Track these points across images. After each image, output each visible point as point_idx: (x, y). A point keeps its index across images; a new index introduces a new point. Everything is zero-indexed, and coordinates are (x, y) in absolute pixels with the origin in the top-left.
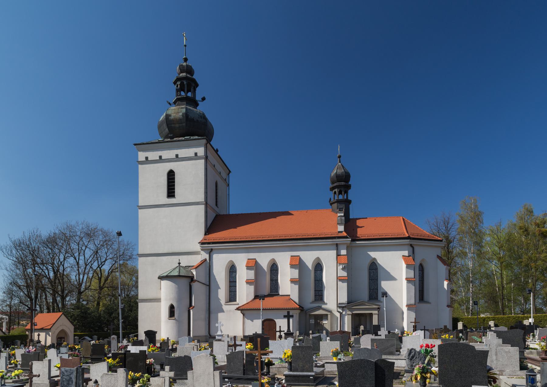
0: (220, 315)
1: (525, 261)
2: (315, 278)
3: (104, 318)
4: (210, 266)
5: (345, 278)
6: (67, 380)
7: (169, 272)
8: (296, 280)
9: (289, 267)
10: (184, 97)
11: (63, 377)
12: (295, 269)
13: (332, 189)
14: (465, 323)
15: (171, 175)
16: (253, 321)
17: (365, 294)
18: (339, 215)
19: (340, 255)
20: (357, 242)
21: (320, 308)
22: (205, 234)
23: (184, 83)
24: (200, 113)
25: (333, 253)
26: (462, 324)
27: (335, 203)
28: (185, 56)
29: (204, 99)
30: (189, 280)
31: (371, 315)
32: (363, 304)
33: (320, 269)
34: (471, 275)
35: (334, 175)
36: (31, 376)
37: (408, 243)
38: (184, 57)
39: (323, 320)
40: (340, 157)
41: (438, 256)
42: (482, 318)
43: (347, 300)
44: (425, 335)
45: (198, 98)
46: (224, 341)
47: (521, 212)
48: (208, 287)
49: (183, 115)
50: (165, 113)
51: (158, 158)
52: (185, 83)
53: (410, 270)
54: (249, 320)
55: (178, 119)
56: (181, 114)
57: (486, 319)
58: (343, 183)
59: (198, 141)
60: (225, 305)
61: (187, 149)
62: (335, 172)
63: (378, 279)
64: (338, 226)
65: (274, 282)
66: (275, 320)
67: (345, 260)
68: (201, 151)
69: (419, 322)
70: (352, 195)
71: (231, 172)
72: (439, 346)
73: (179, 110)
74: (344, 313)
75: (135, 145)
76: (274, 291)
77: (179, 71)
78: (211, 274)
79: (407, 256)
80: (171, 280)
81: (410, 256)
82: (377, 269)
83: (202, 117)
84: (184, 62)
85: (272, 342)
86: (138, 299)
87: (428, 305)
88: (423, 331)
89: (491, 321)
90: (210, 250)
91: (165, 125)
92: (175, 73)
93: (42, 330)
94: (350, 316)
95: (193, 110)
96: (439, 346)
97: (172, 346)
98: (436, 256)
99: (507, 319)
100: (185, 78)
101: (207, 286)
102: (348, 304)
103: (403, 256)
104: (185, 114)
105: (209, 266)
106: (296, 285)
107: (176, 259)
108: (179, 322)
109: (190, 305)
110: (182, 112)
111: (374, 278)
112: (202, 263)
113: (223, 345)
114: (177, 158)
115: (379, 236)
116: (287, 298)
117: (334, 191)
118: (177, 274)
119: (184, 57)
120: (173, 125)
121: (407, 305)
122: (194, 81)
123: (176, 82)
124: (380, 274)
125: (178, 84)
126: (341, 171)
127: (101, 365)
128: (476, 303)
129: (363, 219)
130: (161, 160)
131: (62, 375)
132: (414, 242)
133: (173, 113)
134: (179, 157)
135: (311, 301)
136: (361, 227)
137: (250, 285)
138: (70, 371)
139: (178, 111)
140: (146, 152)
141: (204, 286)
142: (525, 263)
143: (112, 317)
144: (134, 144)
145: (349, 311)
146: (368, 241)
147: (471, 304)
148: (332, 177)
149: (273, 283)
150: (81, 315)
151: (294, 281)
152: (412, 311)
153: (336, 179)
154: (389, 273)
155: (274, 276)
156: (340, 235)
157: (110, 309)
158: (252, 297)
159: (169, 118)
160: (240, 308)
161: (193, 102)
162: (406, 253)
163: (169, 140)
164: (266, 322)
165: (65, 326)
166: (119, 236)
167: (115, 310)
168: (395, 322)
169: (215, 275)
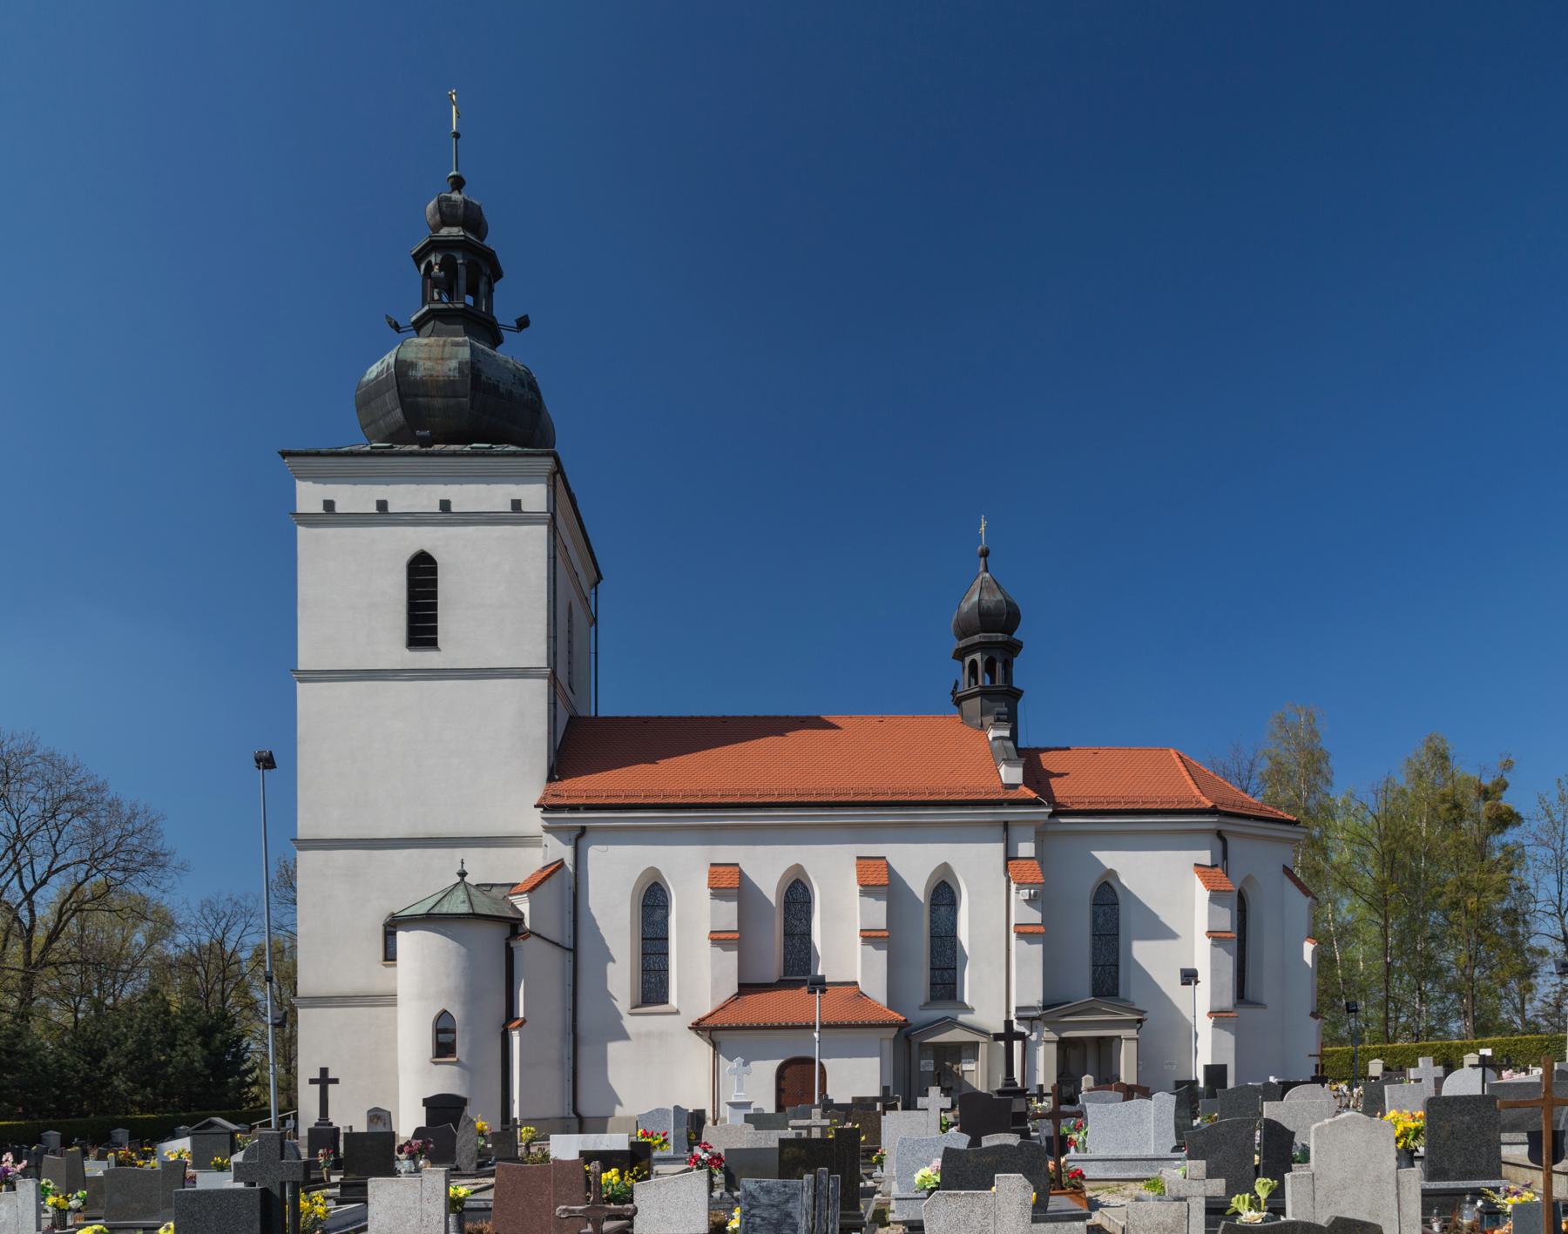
0: (614, 1049)
1: (1451, 892)
2: (931, 929)
3: (73, 1068)
5: (1036, 929)
6: (770, 1223)
8: (880, 934)
11: (752, 1212)
12: (877, 900)
13: (960, 655)
15: (422, 571)
17: (1081, 983)
19: (1017, 858)
21: (952, 1024)
22: (550, 779)
23: (455, 259)
24: (518, 369)
28: (457, 170)
29: (523, 323)
32: (1093, 1008)
33: (948, 901)
35: (971, 609)
36: (599, 1212)
37: (1212, 826)
38: (454, 173)
40: (985, 554)
42: (1348, 1052)
43: (1041, 998)
45: (504, 313)
46: (927, 1109)
47: (1417, 755)
48: (570, 956)
49: (460, 370)
50: (395, 351)
52: (460, 261)
53: (1220, 908)
56: (453, 364)
58: (1000, 637)
60: (630, 1014)
61: (485, 486)
62: (975, 598)
63: (1118, 935)
65: (796, 941)
68: (535, 496)
73: (447, 349)
74: (1034, 1037)
76: (796, 968)
77: (438, 217)
79: (1208, 867)
80: (443, 930)
81: (1216, 866)
83: (526, 384)
85: (1099, 1107)
87: (1260, 1011)
89: (1372, 1059)
90: (578, 832)
91: (390, 398)
94: (1054, 1046)
97: (527, 1147)
101: (567, 952)
102: (1045, 1007)
103: (1196, 865)
104: (470, 365)
105: (572, 883)
109: (507, 1018)
110: (456, 358)
111: (1106, 933)
112: (545, 879)
113: (923, 1120)
115: (1108, 803)
116: (850, 991)
117: (968, 660)
118: (464, 909)
119: (451, 174)
120: (420, 399)
121: (1211, 1014)
122: (490, 257)
123: (420, 255)
124: (1126, 916)
125: (433, 261)
126: (995, 596)
127: (680, 1182)
128: (1355, 1008)
129: (1057, 752)
131: (749, 1204)
132: (1228, 823)
133: (425, 359)
134: (453, 510)
135: (922, 1004)
136: (1060, 775)
137: (725, 950)
138: (783, 1189)
139: (443, 352)
140: (325, 484)
141: (557, 951)
142: (1451, 898)
143: (106, 1066)
145: (1051, 1030)
146: (1095, 818)
149: (793, 945)
152: (1226, 1030)
153: (978, 621)
154: (1156, 917)
155: (797, 922)
156: (1013, 795)
157: (92, 1037)
160: (705, 1024)
161: (484, 328)
162: (1205, 857)
163: (416, 447)
166: (265, 767)
167: (115, 1041)
168: (1171, 1064)
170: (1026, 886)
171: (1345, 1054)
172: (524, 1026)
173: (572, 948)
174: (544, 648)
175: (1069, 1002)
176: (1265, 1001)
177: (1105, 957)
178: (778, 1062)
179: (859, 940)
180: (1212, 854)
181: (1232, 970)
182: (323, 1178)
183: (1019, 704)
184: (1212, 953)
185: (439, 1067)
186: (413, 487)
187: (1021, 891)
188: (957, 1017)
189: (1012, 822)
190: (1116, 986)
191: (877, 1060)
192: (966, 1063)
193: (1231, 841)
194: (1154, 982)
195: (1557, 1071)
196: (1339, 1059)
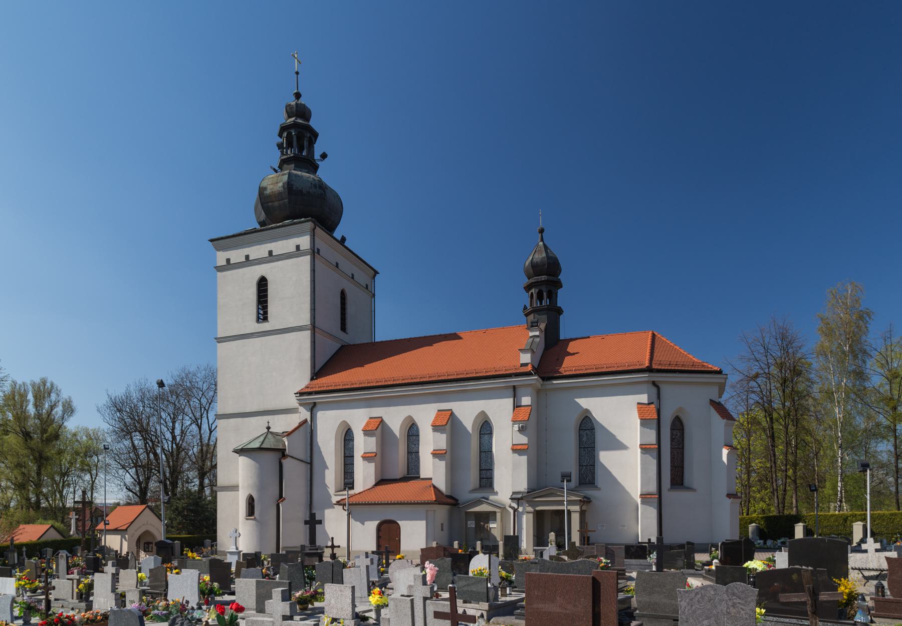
4: (312, 430)
7: (243, 445)
8: (441, 452)
9: (363, 435)
10: (291, 157)
13: (528, 288)
14: (809, 524)
15: (262, 284)
16: (363, 524)
18: (531, 334)
19: (521, 406)
20: (555, 382)
22: (312, 379)
23: (292, 133)
25: (507, 403)
26: (802, 527)
27: (531, 314)
29: (324, 156)
30: (279, 455)
34: (839, 433)
37: (646, 379)
38: (295, 91)
39: (490, 522)
43: (526, 487)
44: (491, 563)
48: (309, 466)
49: (283, 186)
51: (244, 260)
52: (293, 134)
53: (648, 430)
55: (278, 193)
56: (281, 184)
57: (849, 518)
58: (544, 278)
61: (285, 241)
64: (521, 354)
66: (399, 522)
67: (524, 414)
69: (595, 531)
70: (563, 298)
71: (378, 273)
73: (279, 178)
74: (521, 509)
75: (211, 241)
76: (413, 471)
78: (314, 444)
79: (646, 404)
82: (594, 429)
83: (318, 186)
84: (295, 99)
86: (216, 486)
88: (488, 555)
92: (282, 118)
93: (116, 531)
94: (531, 515)
95: (302, 176)
98: (709, 401)
99: (890, 519)
100: (295, 125)
104: (287, 184)
106: (441, 462)
107: (262, 421)
108: (261, 525)
114: (271, 257)
120: (270, 204)
124: (599, 437)
130: (248, 261)
134: (274, 254)
135: (471, 489)
136: (574, 354)
141: (303, 464)
147: (839, 489)
148: (527, 267)
149: (412, 458)
150: (188, 507)
151: (438, 454)
154: (614, 436)
158: (372, 482)
159: (265, 193)
162: (644, 398)
164: (385, 525)
169: (320, 447)
170: (518, 423)
171: (840, 517)
172: (284, 502)
173: (309, 461)
174: (309, 315)
175: (546, 487)
176: (695, 487)
178: (377, 522)
179: (639, 450)
180: (648, 396)
181: (656, 469)
185: (248, 521)
186: (258, 246)
187: (515, 426)
189: (518, 385)
190: (594, 478)
191: (424, 522)
192: (491, 523)
193: (662, 387)
196: (836, 521)
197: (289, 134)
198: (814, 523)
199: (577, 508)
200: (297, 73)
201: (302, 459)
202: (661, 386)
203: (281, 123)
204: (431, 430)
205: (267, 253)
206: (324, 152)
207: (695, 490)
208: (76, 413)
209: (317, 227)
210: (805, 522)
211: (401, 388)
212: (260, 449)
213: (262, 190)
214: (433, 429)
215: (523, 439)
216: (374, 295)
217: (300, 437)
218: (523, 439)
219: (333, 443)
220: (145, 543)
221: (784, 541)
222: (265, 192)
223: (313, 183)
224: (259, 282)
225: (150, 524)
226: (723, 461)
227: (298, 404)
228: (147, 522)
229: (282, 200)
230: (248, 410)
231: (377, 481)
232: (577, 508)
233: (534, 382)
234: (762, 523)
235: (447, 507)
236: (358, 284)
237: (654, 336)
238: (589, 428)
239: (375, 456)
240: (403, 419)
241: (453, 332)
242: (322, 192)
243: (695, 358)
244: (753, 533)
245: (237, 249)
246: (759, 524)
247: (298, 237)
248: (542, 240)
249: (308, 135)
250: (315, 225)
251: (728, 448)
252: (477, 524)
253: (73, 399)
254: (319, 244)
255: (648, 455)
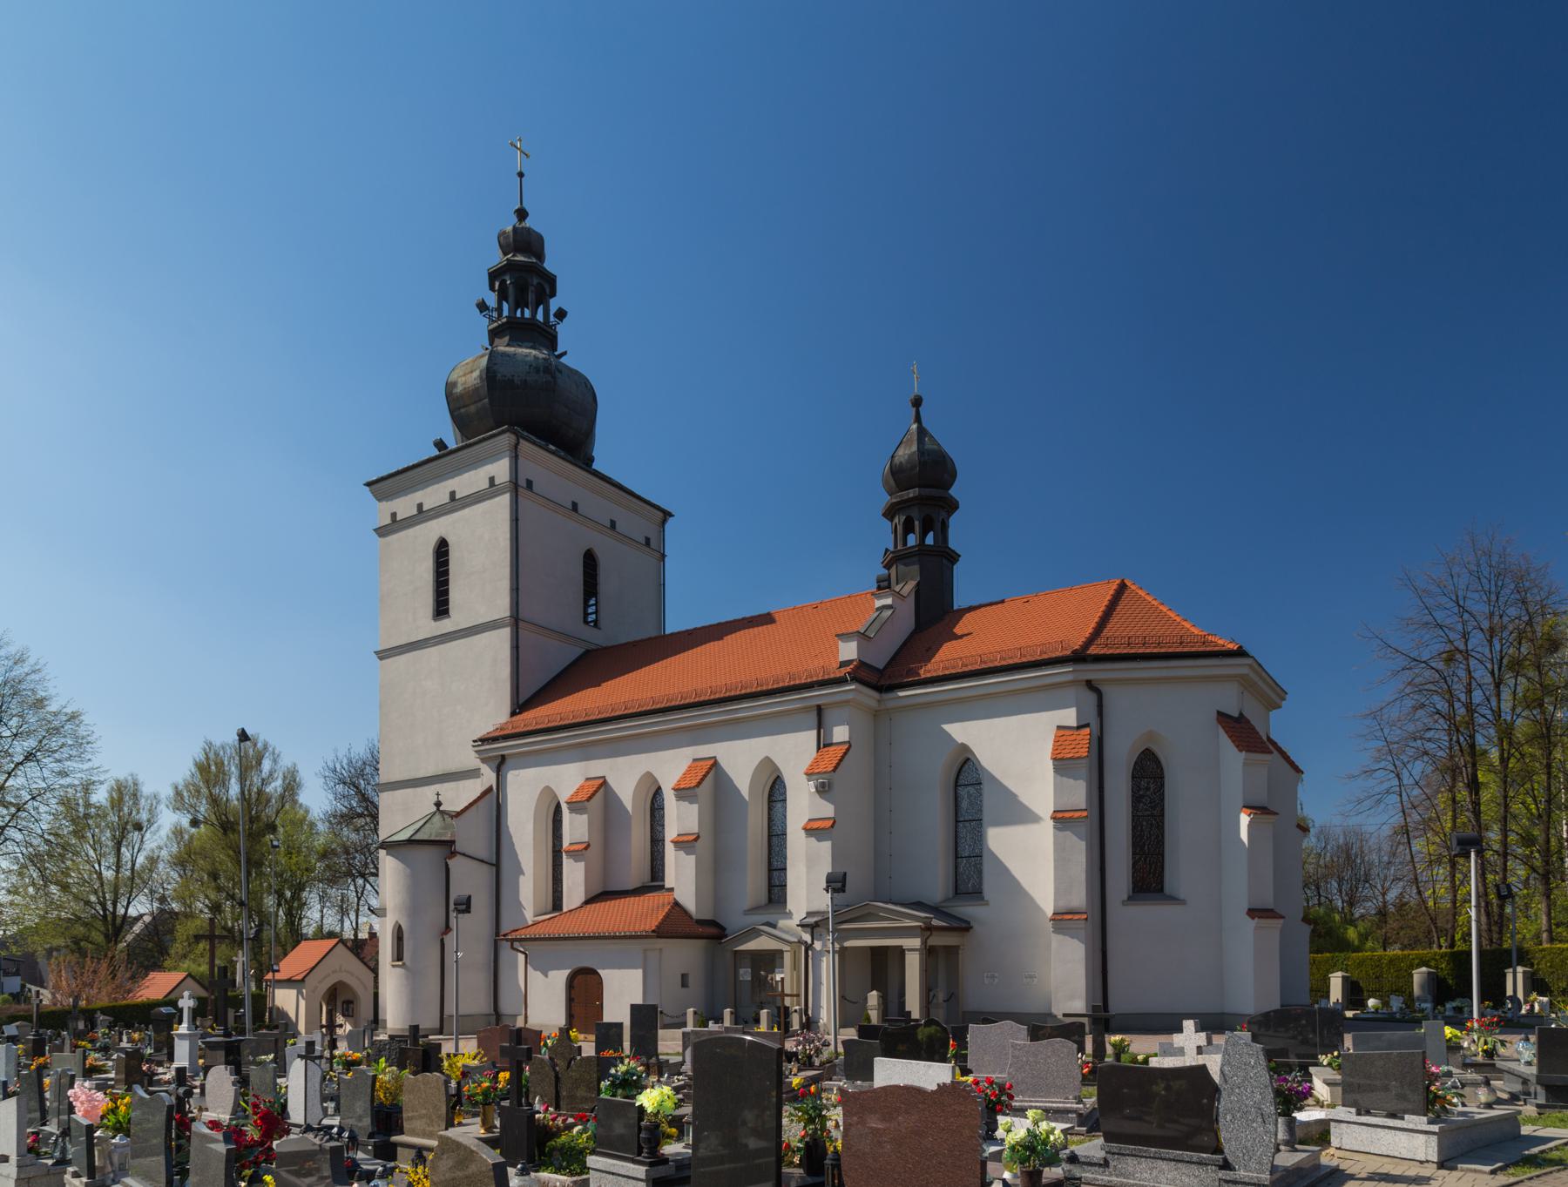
8: (1077, 814)
16: (546, 976)
18: (879, 603)
19: (831, 745)
20: (901, 694)
22: (513, 714)
27: (892, 565)
31: (901, 952)
37: (1070, 677)
39: (777, 970)
41: (1222, 717)
48: (494, 868)
49: (480, 377)
51: (415, 512)
52: (508, 282)
53: (1071, 781)
54: (539, 973)
56: (476, 374)
58: (912, 493)
59: (491, 441)
64: (840, 642)
70: (959, 533)
71: (671, 515)
72: (1204, 1067)
74: (818, 945)
75: (369, 484)
93: (289, 983)
96: (1204, 1067)
98: (1215, 715)
107: (428, 794)
114: (455, 503)
120: (463, 410)
135: (746, 908)
141: (485, 866)
144: (365, 485)
162: (1069, 716)
164: (580, 977)
165: (348, 972)
173: (494, 862)
177: (970, 845)
178: (566, 972)
181: (1084, 860)
182: (521, 1045)
183: (955, 567)
184: (1055, 837)
186: (436, 486)
188: (777, 922)
191: (638, 973)
194: (1014, 878)
195: (859, 1037)
197: (503, 283)
198: (1551, 966)
199: (916, 942)
200: (521, 175)
201: (480, 858)
202: (1105, 689)
203: (487, 268)
204: (673, 797)
205: (448, 496)
206: (560, 308)
207: (1182, 902)
208: (303, 789)
209: (521, 440)
210: (1532, 965)
211: (630, 721)
212: (410, 842)
213: (450, 386)
214: (676, 796)
215: (827, 810)
216: (663, 556)
217: (483, 814)
218: (827, 810)
219: (530, 827)
220: (344, 1002)
221: (1459, 1005)
222: (455, 391)
223: (534, 365)
224: (438, 549)
225: (345, 971)
226: (1241, 840)
227: (478, 760)
228: (340, 969)
229: (480, 400)
230: (422, 774)
231: (589, 897)
232: (916, 942)
233: (850, 696)
234: (1443, 966)
235: (700, 943)
236: (627, 539)
237: (1122, 587)
238: (973, 781)
239: (586, 848)
240: (638, 777)
241: (764, 611)
242: (550, 378)
243: (1194, 630)
244: (1422, 987)
245: (406, 495)
246: (1437, 968)
247: (492, 463)
248: (918, 419)
249: (535, 281)
250: (518, 436)
251: (1249, 811)
252: (755, 975)
253: (299, 767)
254: (528, 470)
255: (1068, 833)
